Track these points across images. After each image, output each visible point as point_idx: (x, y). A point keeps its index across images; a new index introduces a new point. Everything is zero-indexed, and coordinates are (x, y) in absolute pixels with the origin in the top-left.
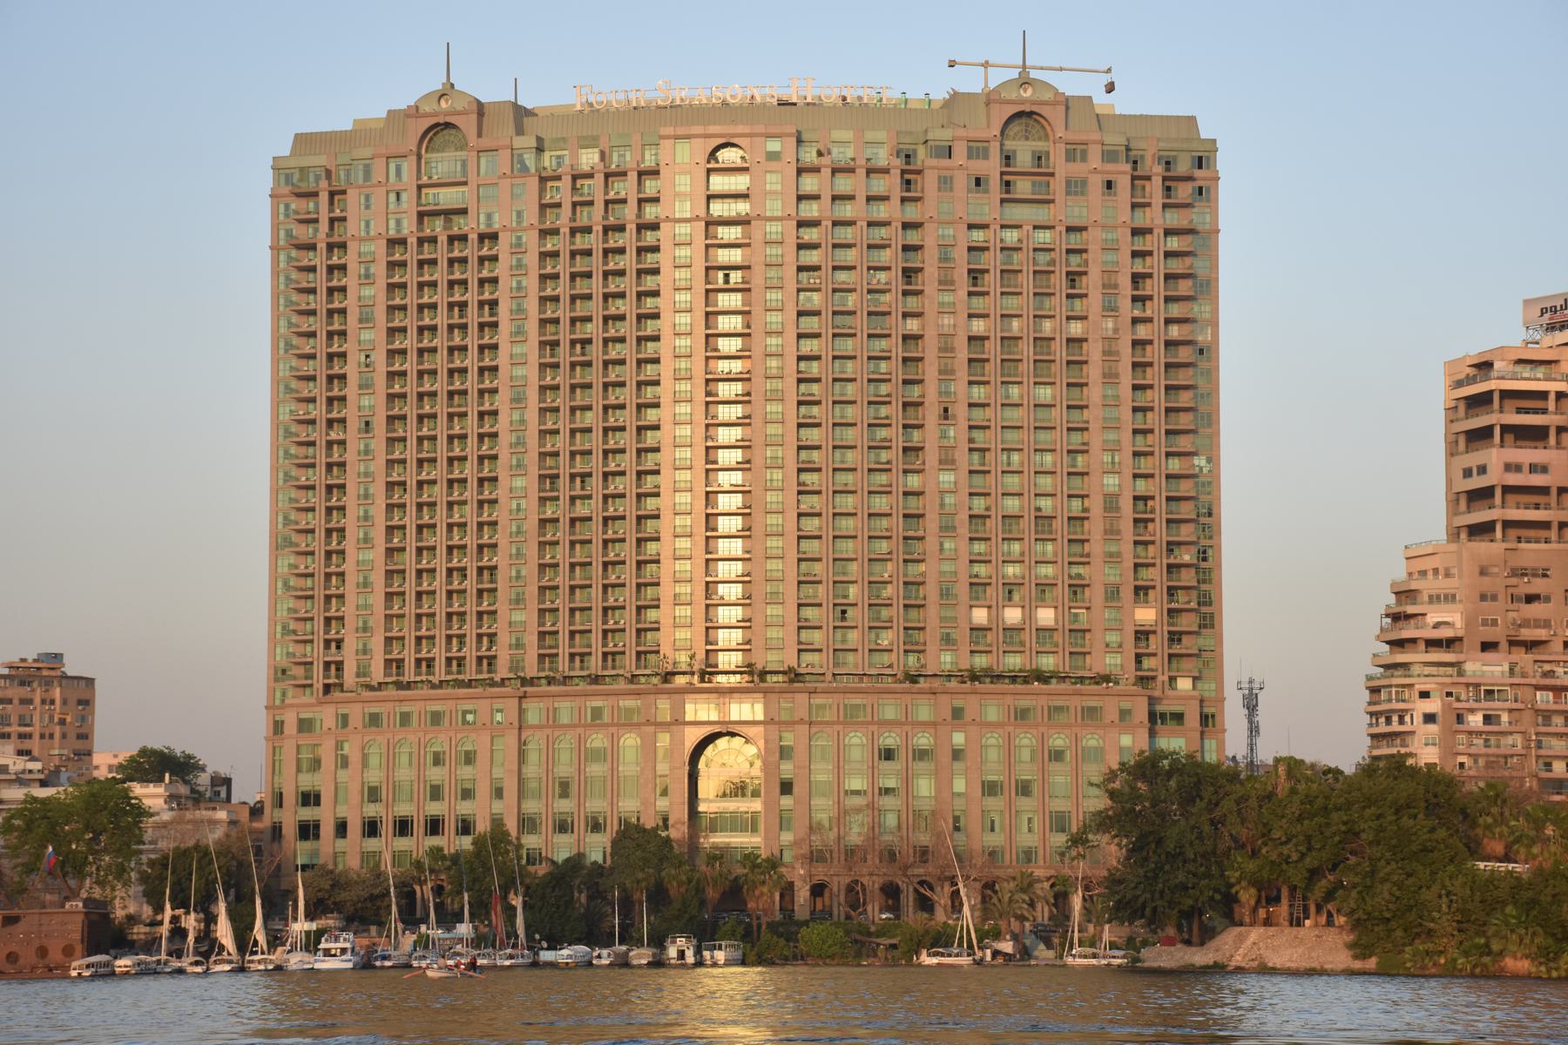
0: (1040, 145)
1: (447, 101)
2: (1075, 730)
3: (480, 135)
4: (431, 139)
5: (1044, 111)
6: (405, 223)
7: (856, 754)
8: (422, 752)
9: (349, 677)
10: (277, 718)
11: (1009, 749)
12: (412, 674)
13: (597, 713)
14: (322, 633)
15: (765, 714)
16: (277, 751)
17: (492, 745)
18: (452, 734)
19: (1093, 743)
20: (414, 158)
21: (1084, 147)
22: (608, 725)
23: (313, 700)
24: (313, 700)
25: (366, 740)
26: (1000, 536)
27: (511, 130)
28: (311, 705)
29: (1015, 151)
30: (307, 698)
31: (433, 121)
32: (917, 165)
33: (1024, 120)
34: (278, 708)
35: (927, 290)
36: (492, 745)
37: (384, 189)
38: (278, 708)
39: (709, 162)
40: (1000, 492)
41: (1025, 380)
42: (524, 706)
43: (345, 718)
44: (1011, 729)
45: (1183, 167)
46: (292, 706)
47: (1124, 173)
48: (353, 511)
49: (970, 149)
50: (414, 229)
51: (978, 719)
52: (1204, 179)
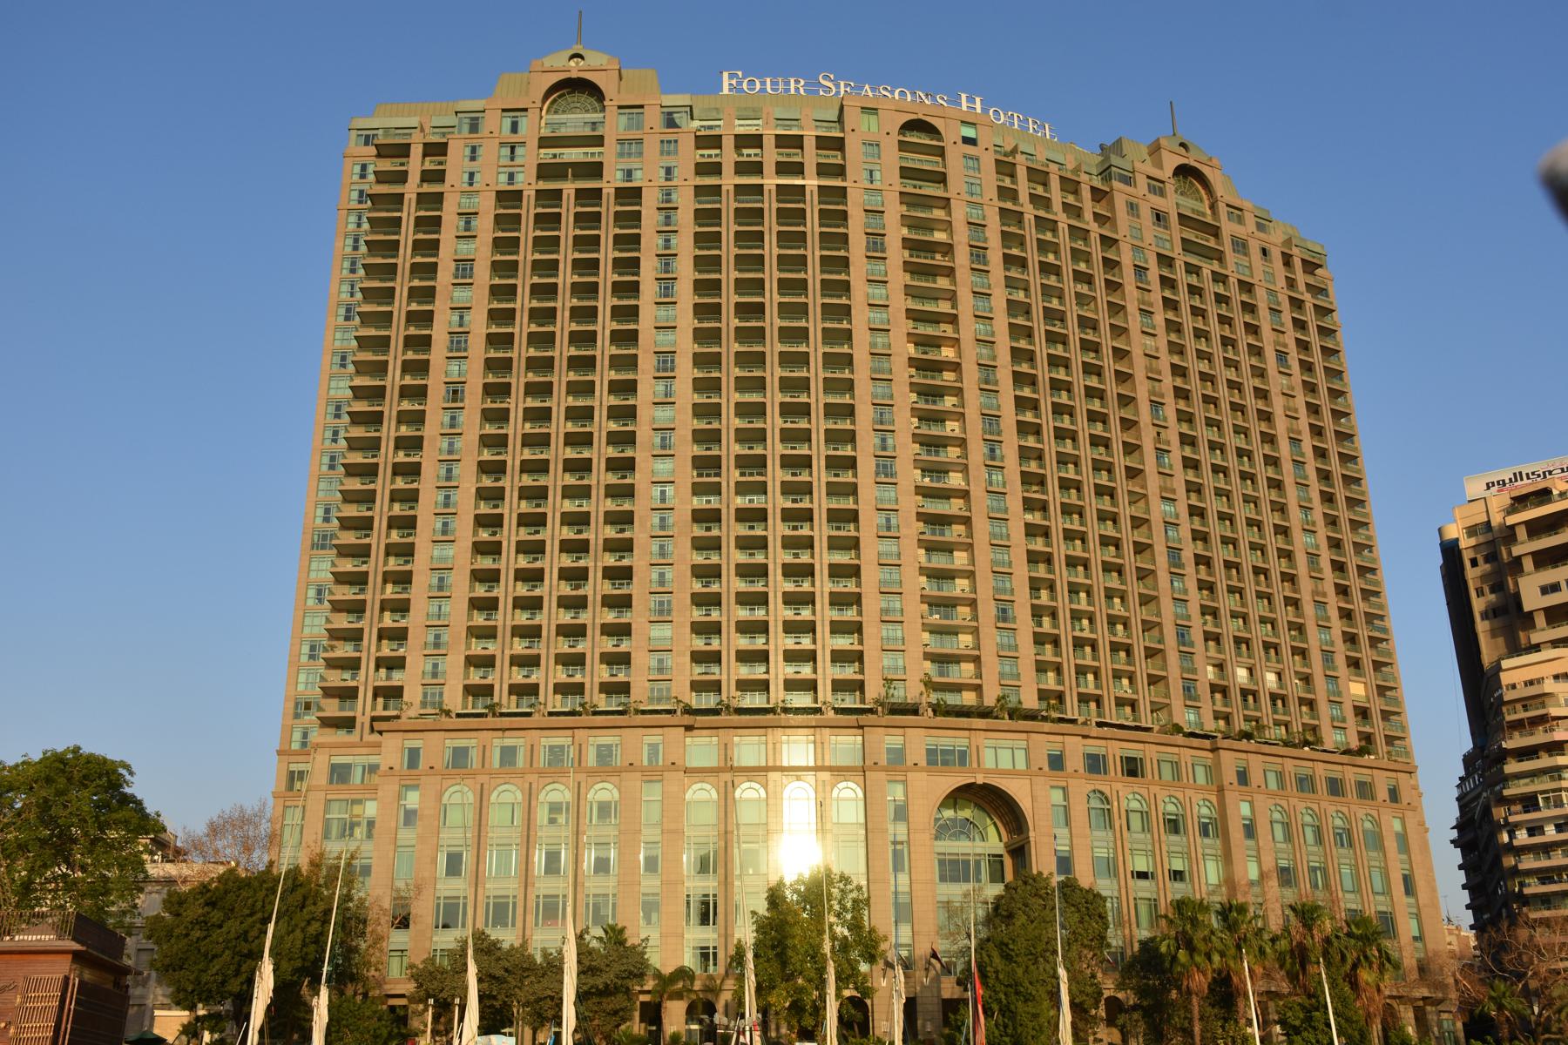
1: (577, 63)
4: (554, 101)
6: (519, 178)
34: (296, 753)
36: (325, 812)
37: (497, 141)
38: (296, 753)
46: (317, 746)
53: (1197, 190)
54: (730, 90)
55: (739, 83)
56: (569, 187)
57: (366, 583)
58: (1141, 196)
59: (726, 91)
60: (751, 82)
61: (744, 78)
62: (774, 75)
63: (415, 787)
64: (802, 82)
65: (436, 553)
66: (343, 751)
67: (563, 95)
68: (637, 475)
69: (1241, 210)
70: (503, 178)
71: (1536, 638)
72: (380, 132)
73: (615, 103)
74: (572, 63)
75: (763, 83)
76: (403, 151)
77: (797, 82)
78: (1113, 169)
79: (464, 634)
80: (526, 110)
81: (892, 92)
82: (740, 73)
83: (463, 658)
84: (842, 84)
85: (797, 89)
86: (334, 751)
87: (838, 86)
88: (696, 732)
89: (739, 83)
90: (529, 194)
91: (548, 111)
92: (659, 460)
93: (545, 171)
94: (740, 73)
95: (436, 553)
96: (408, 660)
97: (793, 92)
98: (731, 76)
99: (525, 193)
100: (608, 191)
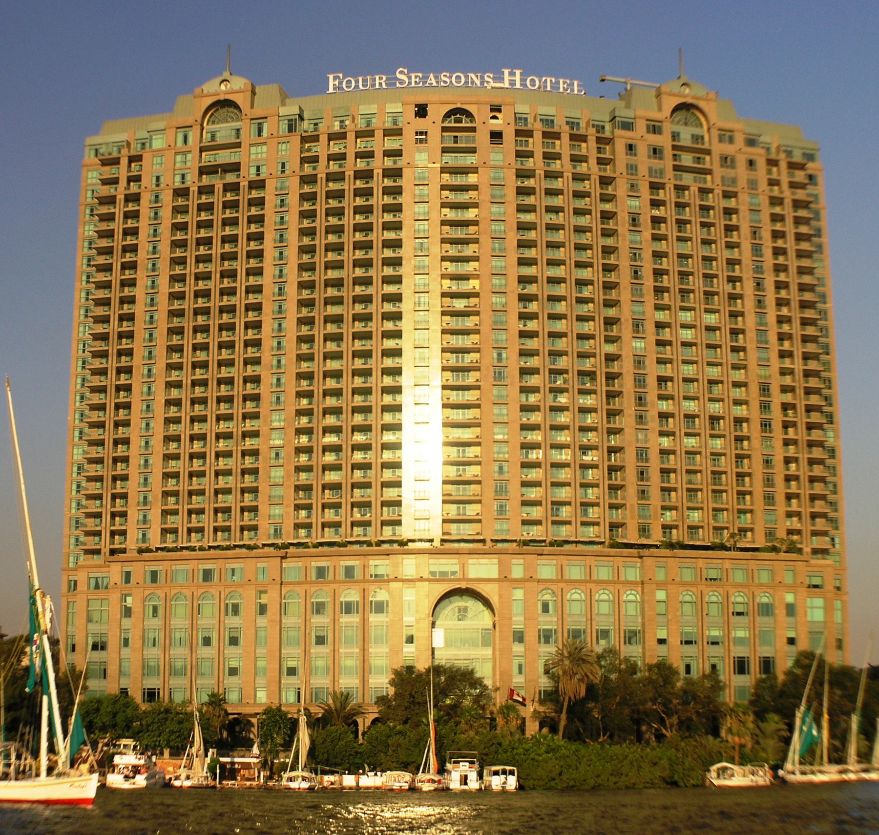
0: (697, 131)
1: (226, 86)
2: (701, 587)
3: (252, 107)
4: (212, 114)
5: (702, 104)
6: (188, 177)
7: (714, 610)
8: (168, 605)
9: (132, 543)
10: (71, 578)
11: (617, 603)
12: (185, 541)
13: (349, 571)
14: (109, 506)
15: (500, 572)
16: (71, 604)
17: (88, 606)
18: (221, 588)
19: (765, 600)
20: (199, 127)
21: (731, 134)
22: (330, 582)
23: (101, 562)
24: (101, 562)
25: (146, 595)
26: (683, 431)
27: (278, 103)
28: (100, 566)
29: (649, 157)
30: (96, 560)
31: (215, 99)
32: (607, 134)
33: (684, 112)
34: (72, 570)
35: (620, 230)
36: (88, 606)
37: (173, 151)
38: (72, 570)
39: (443, 122)
40: (681, 395)
41: (697, 306)
42: (284, 565)
43: (128, 574)
44: (703, 588)
45: (797, 158)
46: (83, 567)
47: (760, 155)
48: (134, 516)
49: (648, 126)
50: (196, 181)
51: (678, 579)
52: (813, 169)
53: (698, 118)
54: (334, 89)
55: (341, 83)
56: (218, 182)
57: (315, 252)
58: (639, 137)
59: (331, 90)
60: (349, 82)
61: (344, 78)
62: (364, 75)
63: (130, 595)
64: (384, 78)
65: (417, 192)
66: (95, 570)
67: (218, 110)
68: (262, 387)
69: (732, 131)
70: (178, 178)
71: (38, 662)
72: (104, 146)
73: (249, 116)
74: (223, 87)
75: (357, 82)
76: (116, 162)
77: (381, 79)
78: (617, 119)
79: (160, 495)
80: (191, 126)
81: (451, 77)
82: (341, 76)
83: (160, 511)
84: (413, 76)
85: (380, 84)
86: (90, 570)
87: (410, 78)
88: (289, 560)
89: (341, 83)
90: (194, 189)
91: (208, 124)
92: (495, 205)
93: (203, 171)
94: (341, 76)
95: (417, 192)
96: (129, 513)
97: (377, 86)
98: (335, 78)
99: (191, 189)
100: (244, 184)
